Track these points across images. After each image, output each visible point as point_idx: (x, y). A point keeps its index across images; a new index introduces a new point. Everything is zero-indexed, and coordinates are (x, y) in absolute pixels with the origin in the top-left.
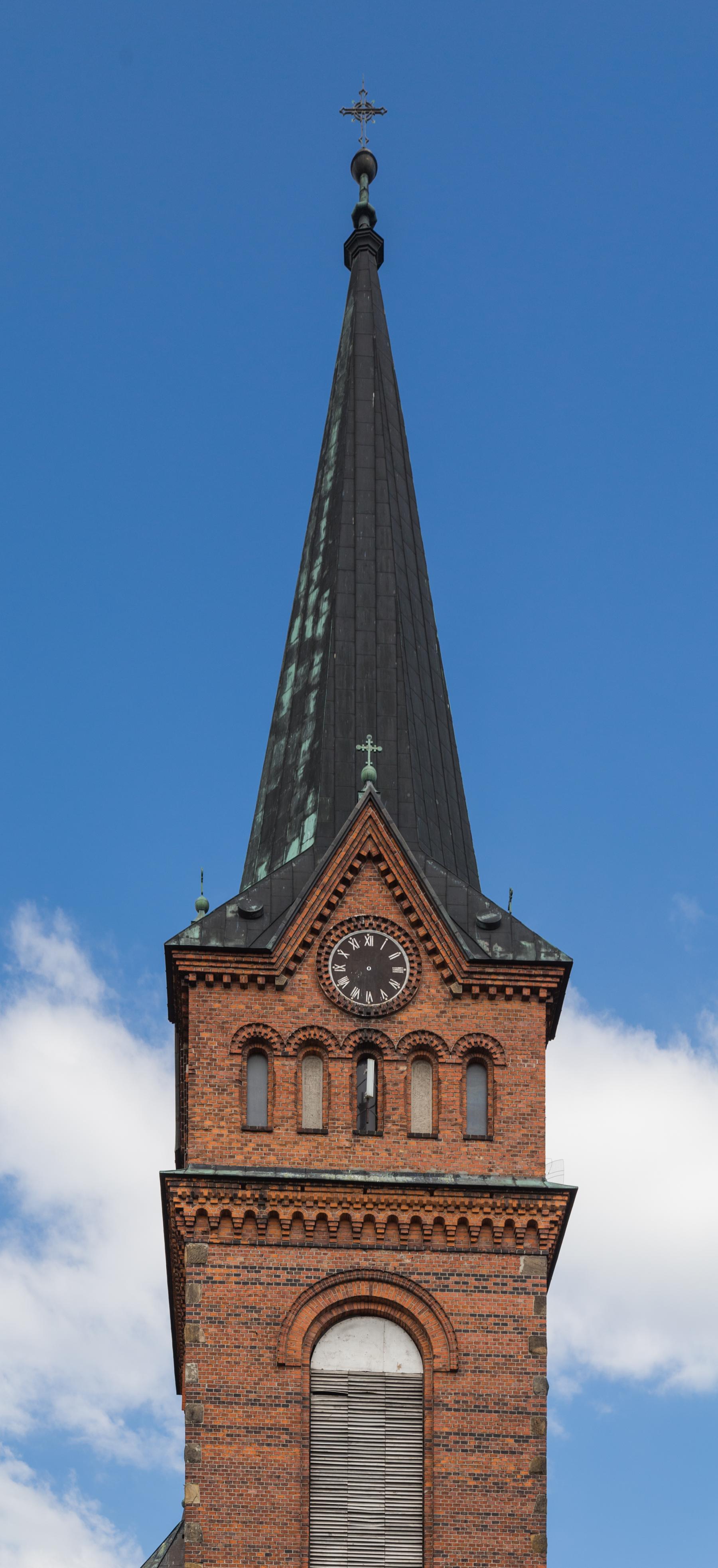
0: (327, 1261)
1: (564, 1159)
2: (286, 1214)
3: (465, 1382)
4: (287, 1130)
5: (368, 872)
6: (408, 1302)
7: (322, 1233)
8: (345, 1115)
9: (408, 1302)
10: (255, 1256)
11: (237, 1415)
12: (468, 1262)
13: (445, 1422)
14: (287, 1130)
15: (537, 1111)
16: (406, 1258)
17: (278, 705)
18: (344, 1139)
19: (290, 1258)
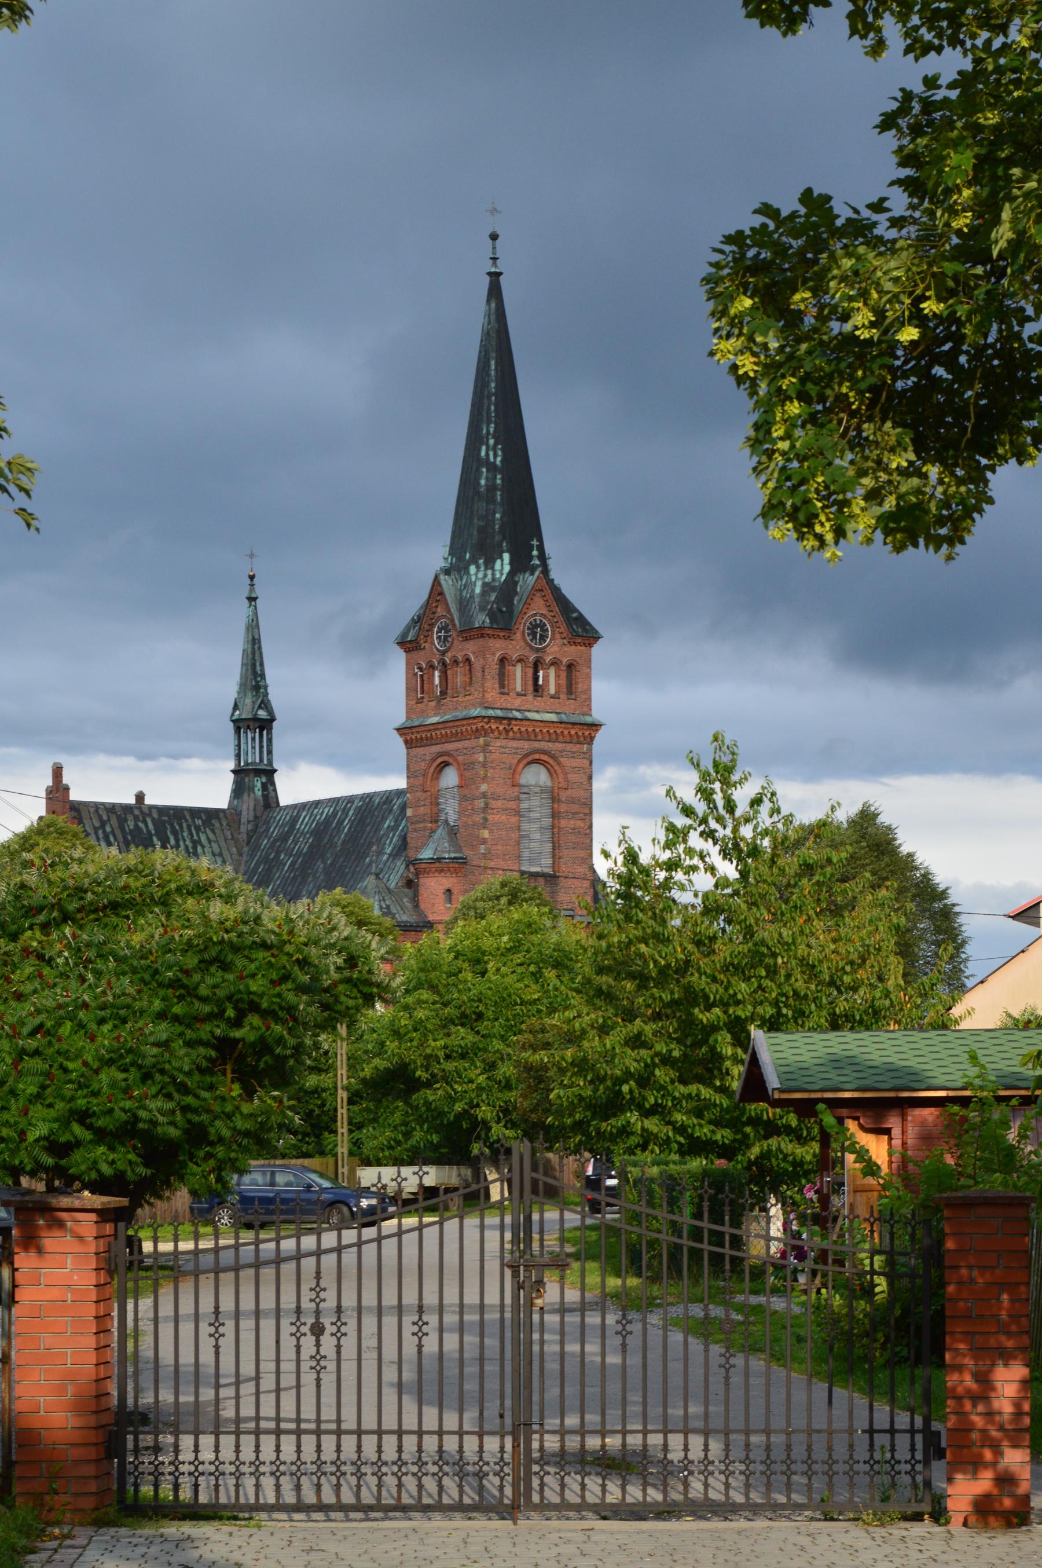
0: (525, 745)
1: (597, 713)
2: (516, 729)
3: (569, 792)
4: (498, 970)
5: (538, 594)
6: (551, 761)
7: (526, 737)
8: (531, 689)
9: (551, 761)
10: (504, 743)
11: (499, 804)
12: (569, 747)
13: (563, 808)
14: (498, 970)
15: (589, 688)
16: (550, 744)
17: (429, 1199)
18: (530, 698)
19: (514, 744)
